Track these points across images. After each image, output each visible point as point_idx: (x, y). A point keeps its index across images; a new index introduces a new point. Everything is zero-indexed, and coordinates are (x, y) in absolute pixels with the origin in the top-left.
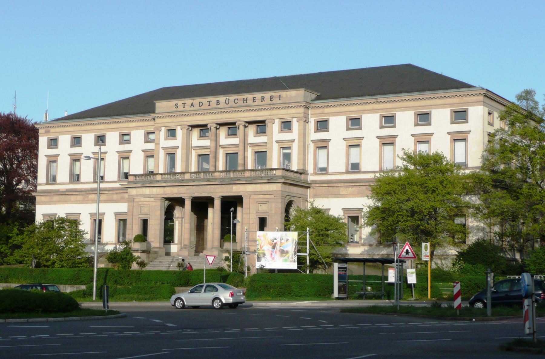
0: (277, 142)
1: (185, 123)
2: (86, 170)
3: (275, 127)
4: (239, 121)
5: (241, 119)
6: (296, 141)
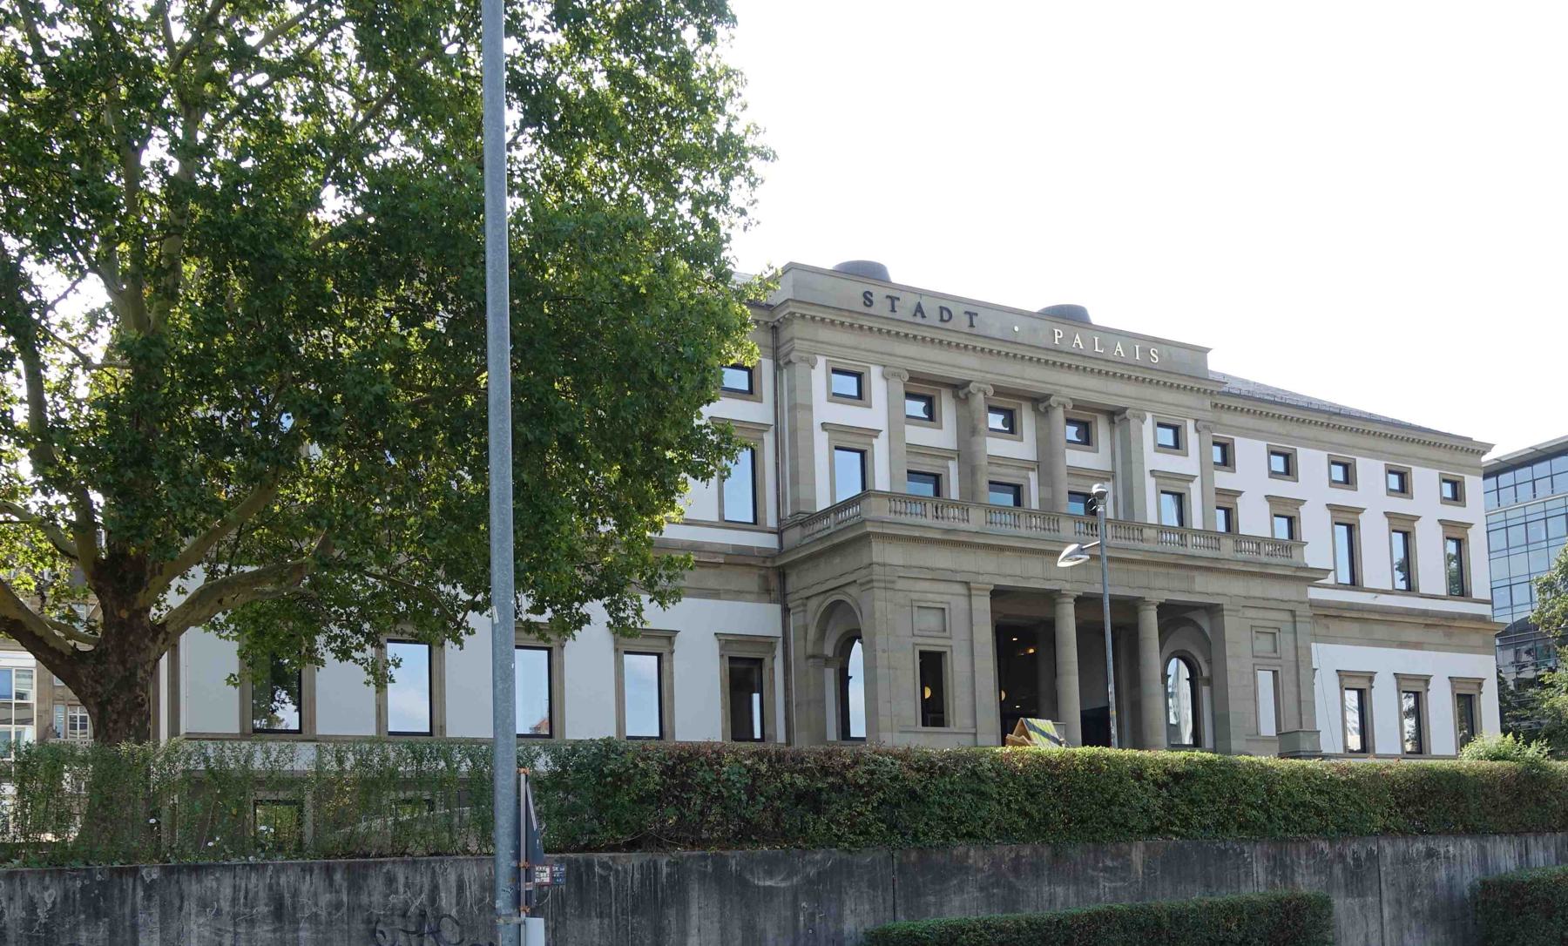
1: (899, 362)
5: (1065, 391)
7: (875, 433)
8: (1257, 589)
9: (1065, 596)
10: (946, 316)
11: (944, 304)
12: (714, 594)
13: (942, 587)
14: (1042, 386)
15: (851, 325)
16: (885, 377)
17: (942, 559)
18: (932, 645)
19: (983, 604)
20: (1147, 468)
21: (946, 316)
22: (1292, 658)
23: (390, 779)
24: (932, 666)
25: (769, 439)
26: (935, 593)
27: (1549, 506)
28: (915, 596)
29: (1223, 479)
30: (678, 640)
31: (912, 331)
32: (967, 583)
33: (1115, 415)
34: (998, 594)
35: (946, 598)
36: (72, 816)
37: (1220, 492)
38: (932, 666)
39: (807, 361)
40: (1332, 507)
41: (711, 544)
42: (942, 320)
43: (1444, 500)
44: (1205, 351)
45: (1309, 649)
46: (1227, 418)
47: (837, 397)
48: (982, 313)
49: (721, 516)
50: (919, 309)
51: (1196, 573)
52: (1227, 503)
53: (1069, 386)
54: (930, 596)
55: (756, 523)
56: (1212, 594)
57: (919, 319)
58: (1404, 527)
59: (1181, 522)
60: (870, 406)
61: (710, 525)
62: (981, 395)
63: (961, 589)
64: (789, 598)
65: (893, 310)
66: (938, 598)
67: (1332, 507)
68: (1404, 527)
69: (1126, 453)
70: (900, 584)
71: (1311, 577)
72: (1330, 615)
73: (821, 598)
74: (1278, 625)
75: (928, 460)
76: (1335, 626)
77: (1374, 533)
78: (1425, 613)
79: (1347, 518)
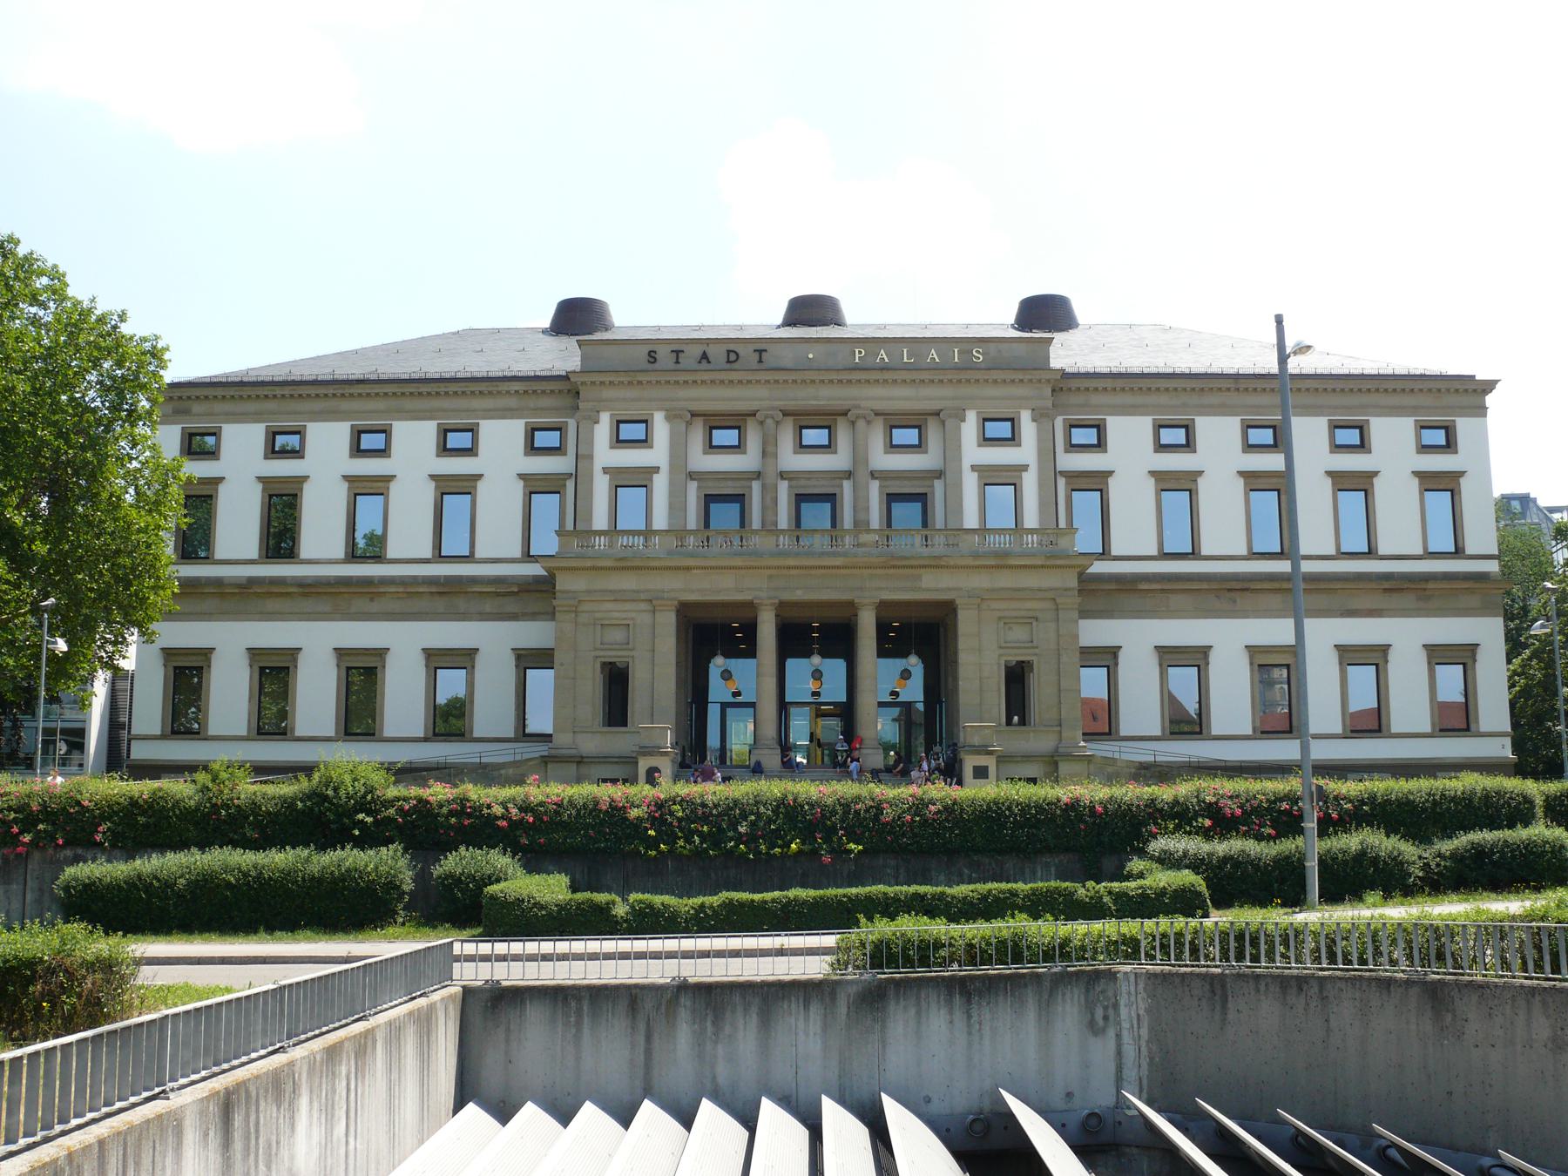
0: (606, 470)
2: (237, 531)
4: (858, 407)
7: (1025, 468)
11: (732, 347)
12: (514, 617)
13: (628, 606)
15: (630, 383)
16: (668, 418)
17: (627, 582)
20: (966, 465)
24: (616, 681)
25: (570, 485)
28: (598, 615)
30: (1122, 656)
31: (672, 378)
36: (1319, 788)
38: (616, 681)
39: (589, 417)
40: (1418, 474)
47: (986, 441)
49: (1425, 547)
50: (705, 356)
51: (922, 571)
55: (528, 556)
57: (704, 365)
59: (834, 524)
61: (252, 562)
66: (624, 615)
67: (1418, 474)
69: (952, 448)
75: (730, 483)
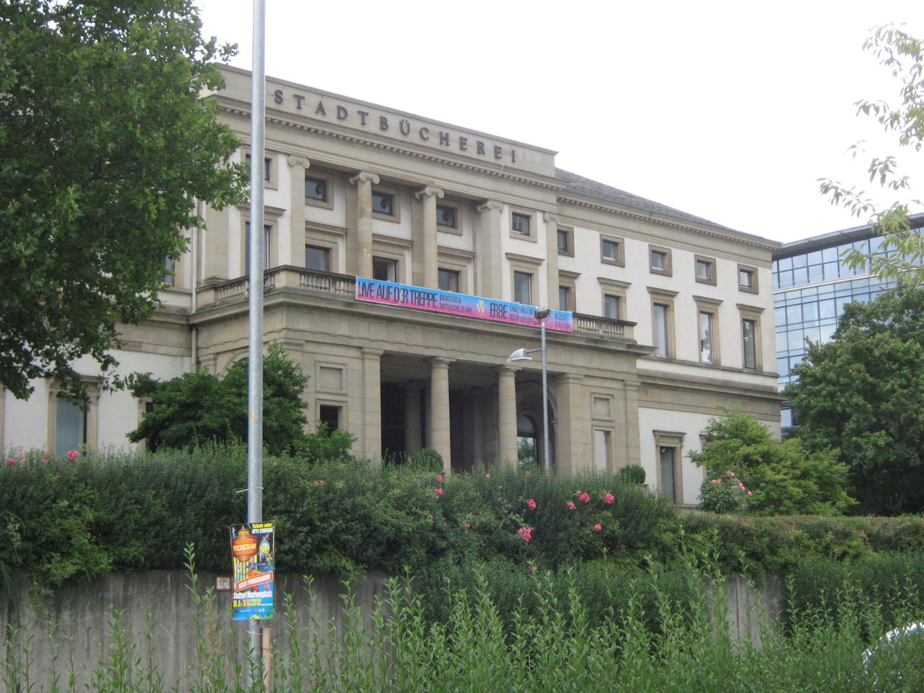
1: (303, 152)
3: (501, 221)
5: (437, 182)
6: (288, 213)
8: (596, 362)
9: (440, 362)
10: (342, 115)
14: (396, 175)
17: (343, 328)
18: (331, 400)
19: (374, 369)
21: (342, 115)
22: (623, 421)
23: (602, 506)
26: (334, 356)
27: (805, 293)
29: (565, 263)
32: (360, 348)
33: (476, 205)
34: (387, 358)
35: (345, 360)
37: (563, 274)
41: (731, 382)
42: (339, 118)
43: (742, 289)
44: (552, 154)
45: (636, 413)
46: (569, 211)
48: (519, 152)
52: (566, 285)
53: (371, 164)
54: (332, 359)
56: (560, 365)
57: (319, 117)
58: (708, 308)
60: (573, 256)
62: (368, 184)
63: (356, 353)
64: (202, 352)
65: (363, 123)
66: (338, 360)
67: (698, 299)
68: (708, 308)
70: (309, 348)
71: (634, 351)
72: (650, 383)
73: (231, 355)
74: (611, 392)
76: (655, 394)
77: (685, 312)
78: (725, 385)
79: (662, 300)
